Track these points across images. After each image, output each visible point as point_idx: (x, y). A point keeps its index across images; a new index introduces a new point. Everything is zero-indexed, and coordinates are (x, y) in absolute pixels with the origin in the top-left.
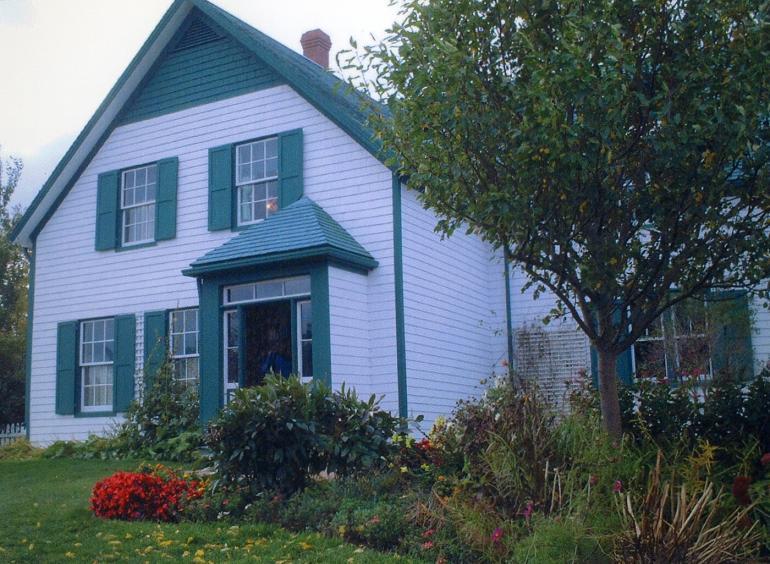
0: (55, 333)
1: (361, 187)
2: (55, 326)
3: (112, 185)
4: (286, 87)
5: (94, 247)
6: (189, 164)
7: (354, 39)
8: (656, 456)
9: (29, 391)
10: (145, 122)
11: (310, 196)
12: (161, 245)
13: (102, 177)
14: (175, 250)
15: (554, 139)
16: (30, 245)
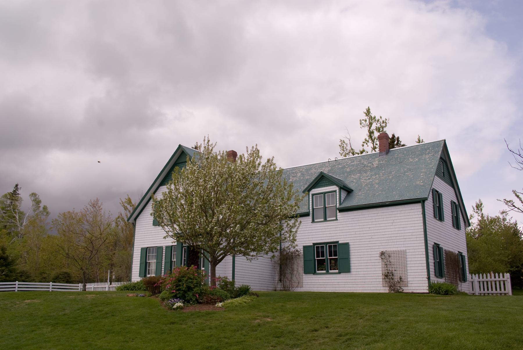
0: (140, 251)
2: (140, 249)
5: (152, 224)
9: (339, 189)
15: (257, 211)
16: (134, 222)
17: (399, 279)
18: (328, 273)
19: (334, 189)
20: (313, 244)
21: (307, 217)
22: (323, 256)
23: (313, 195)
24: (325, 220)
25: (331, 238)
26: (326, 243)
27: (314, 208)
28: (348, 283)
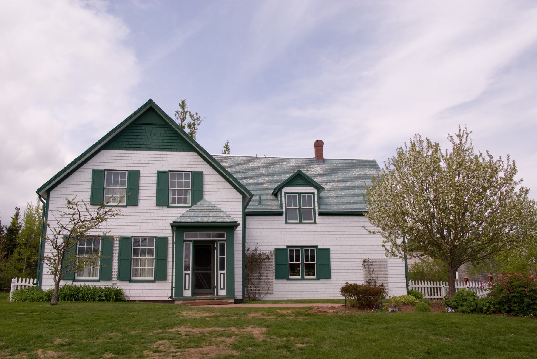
1: (228, 199)
3: (98, 175)
4: (195, 153)
6: (145, 175)
7: (501, 157)
8: (25, 271)
10: (135, 152)
11: (206, 199)
12: (128, 207)
13: (95, 171)
14: (137, 211)
18: (303, 279)
21: (280, 217)
22: (298, 260)
23: (286, 193)
24: (300, 222)
25: (308, 242)
27: (287, 207)
28: (328, 290)
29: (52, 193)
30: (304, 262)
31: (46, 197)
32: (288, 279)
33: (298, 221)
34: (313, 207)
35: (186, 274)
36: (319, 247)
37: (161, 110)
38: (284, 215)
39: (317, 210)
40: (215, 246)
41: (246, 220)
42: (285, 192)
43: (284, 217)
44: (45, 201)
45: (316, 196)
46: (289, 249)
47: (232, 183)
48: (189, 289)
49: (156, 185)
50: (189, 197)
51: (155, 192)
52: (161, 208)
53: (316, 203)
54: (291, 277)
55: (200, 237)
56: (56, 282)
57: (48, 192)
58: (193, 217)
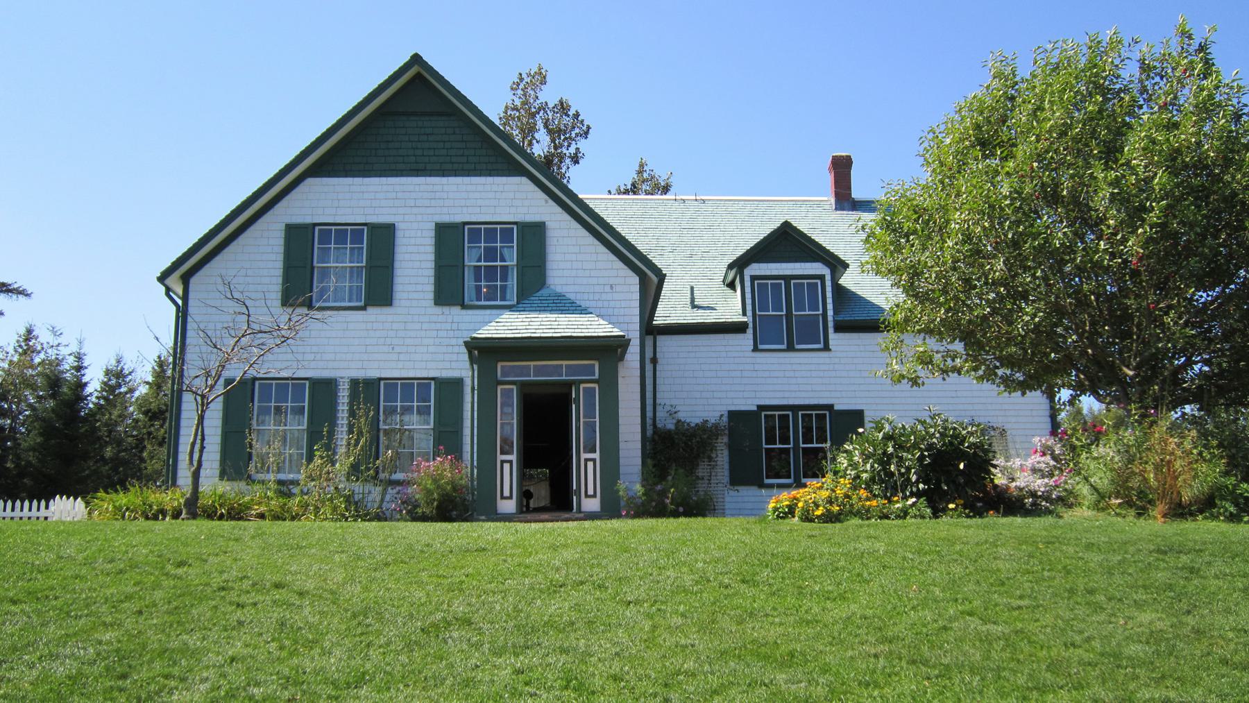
4: (524, 180)
10: (384, 180)
12: (371, 310)
17: (520, 676)
19: (818, 272)
20: (758, 406)
21: (741, 336)
22: (785, 440)
23: (753, 278)
24: (791, 348)
26: (795, 408)
29: (194, 281)
30: (802, 445)
31: (180, 292)
32: (762, 485)
33: (784, 347)
34: (821, 312)
35: (503, 462)
36: (836, 408)
37: (443, 77)
38: (750, 331)
39: (830, 319)
40: (574, 396)
41: (658, 344)
42: (751, 276)
43: (751, 336)
44: (180, 302)
45: (828, 283)
46: (763, 414)
47: (564, 202)
48: (511, 497)
49: (432, 257)
50: (513, 282)
51: (432, 272)
52: (446, 309)
53: (829, 300)
54: (767, 481)
55: (535, 371)
56: (193, 469)
57: (186, 279)
58: (519, 328)
